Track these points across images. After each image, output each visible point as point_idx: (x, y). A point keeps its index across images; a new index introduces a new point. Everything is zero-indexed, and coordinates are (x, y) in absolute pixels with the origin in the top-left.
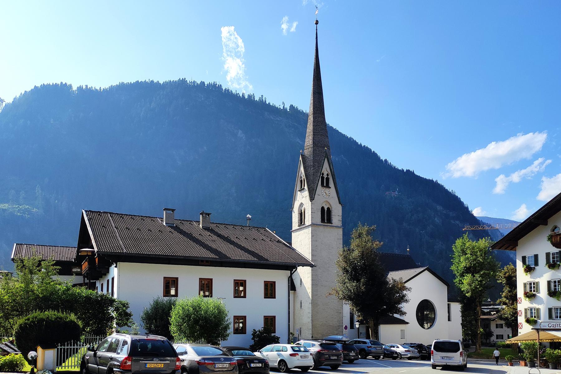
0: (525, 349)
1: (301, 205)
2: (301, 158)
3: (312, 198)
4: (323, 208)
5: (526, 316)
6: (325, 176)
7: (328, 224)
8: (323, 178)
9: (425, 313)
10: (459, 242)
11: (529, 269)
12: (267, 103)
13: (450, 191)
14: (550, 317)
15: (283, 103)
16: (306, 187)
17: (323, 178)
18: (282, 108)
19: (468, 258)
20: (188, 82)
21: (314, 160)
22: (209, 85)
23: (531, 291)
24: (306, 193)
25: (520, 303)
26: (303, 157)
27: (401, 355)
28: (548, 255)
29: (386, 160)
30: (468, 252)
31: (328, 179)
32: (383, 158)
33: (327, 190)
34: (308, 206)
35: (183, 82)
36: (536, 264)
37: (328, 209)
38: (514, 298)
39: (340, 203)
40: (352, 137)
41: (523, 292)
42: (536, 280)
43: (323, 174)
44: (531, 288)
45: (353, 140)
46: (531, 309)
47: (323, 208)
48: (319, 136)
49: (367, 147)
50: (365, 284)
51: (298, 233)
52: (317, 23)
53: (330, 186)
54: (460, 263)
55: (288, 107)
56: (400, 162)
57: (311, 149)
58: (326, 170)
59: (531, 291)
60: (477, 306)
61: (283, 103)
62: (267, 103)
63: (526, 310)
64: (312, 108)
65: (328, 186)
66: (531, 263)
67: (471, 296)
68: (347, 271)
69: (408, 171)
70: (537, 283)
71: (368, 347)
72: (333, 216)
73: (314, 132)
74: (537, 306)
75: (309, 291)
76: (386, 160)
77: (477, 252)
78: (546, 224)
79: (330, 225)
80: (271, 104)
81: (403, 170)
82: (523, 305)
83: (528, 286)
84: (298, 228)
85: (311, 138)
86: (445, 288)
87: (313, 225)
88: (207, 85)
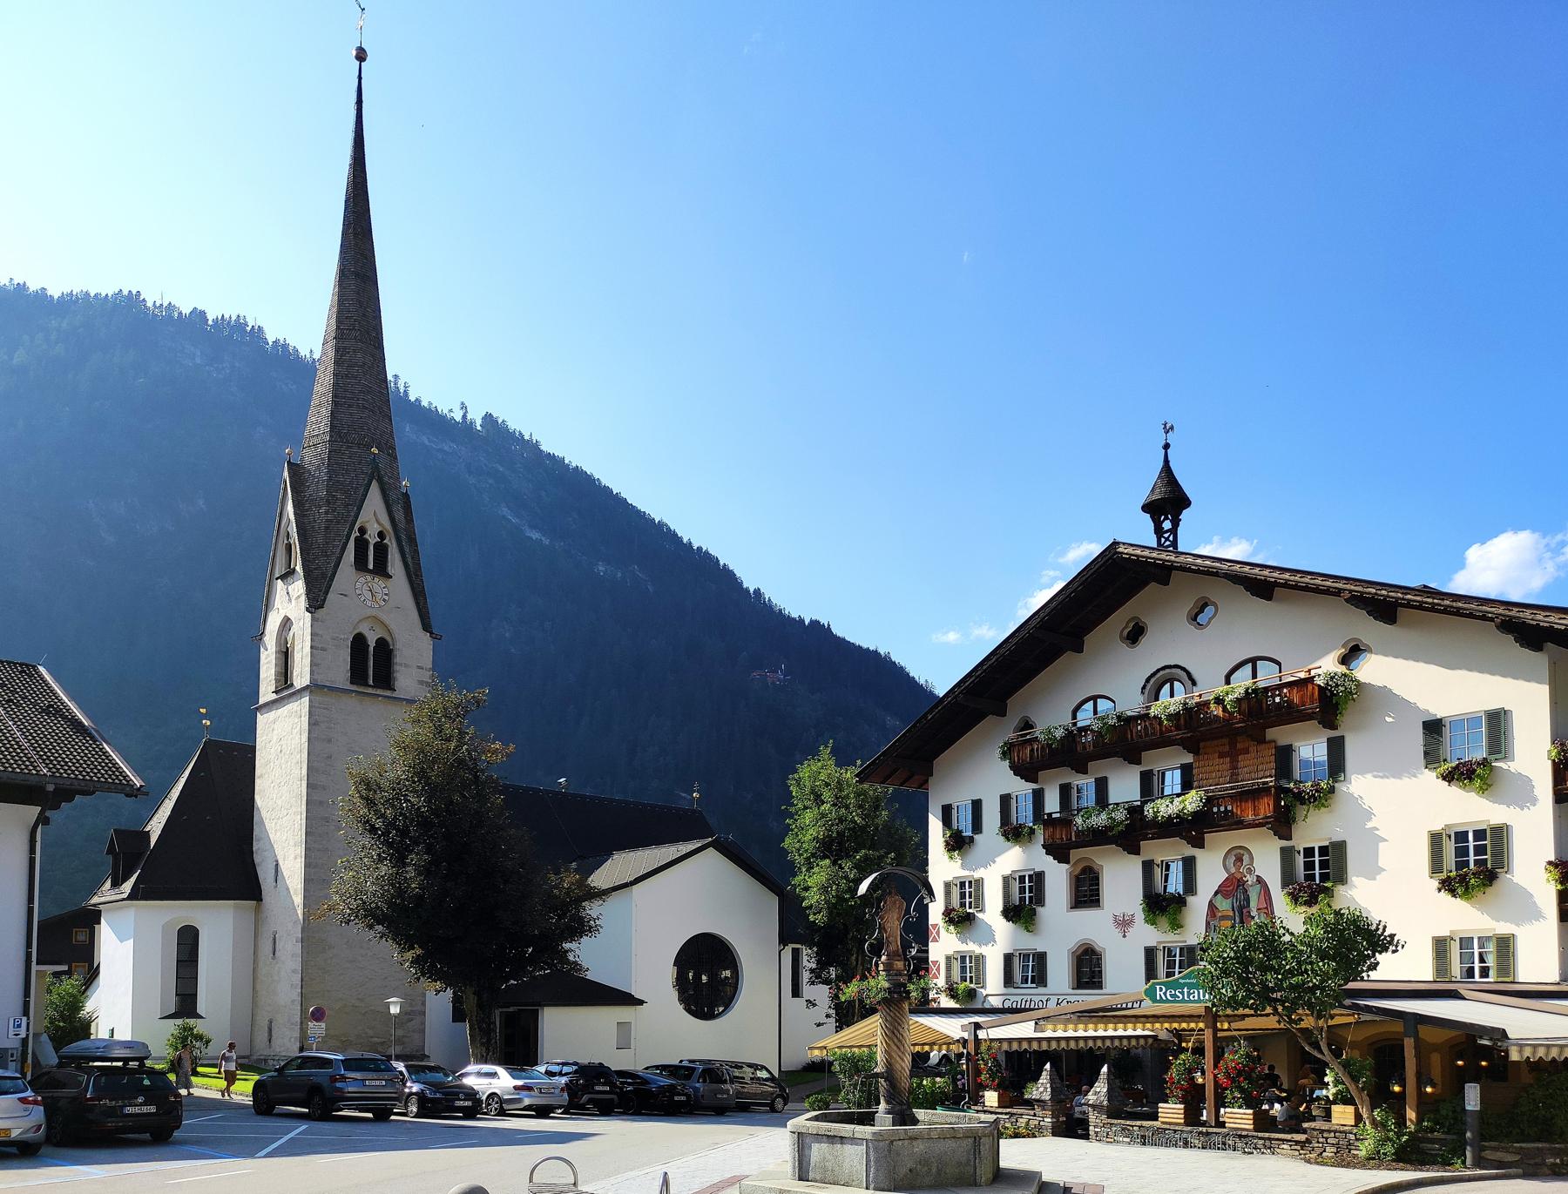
0: (843, 1071)
1: (286, 623)
2: (286, 474)
3: (315, 602)
4: (359, 642)
5: (948, 977)
6: (372, 538)
7: (379, 692)
8: (361, 545)
9: (706, 974)
10: (805, 771)
11: (958, 843)
12: (412, 398)
13: (922, 682)
14: (1008, 980)
15: (463, 406)
16: (299, 568)
17: (361, 545)
18: (458, 418)
19: (823, 815)
20: (150, 304)
21: (332, 484)
22: (221, 323)
23: (963, 905)
24: (298, 587)
25: (935, 940)
26: (296, 470)
27: (501, 1101)
28: (1005, 800)
29: (757, 591)
30: (827, 795)
31: (381, 550)
32: (750, 584)
33: (378, 583)
34: (303, 625)
35: (129, 304)
36: (977, 826)
37: (382, 644)
38: (919, 931)
39: (426, 627)
40: (665, 520)
41: (942, 909)
42: (977, 875)
43: (362, 530)
44: (963, 895)
45: (669, 529)
46: (963, 958)
47: (359, 642)
48: (354, 410)
49: (707, 553)
50: (426, 871)
51: (272, 715)
52: (361, 56)
53: (390, 570)
54: (808, 828)
55: (476, 416)
56: (796, 598)
57: (323, 450)
58: (373, 515)
59: (963, 905)
60: (850, 952)
61: (463, 406)
62: (412, 398)
63: (948, 959)
64: (333, 321)
65: (381, 570)
66: (964, 823)
67: (828, 927)
68: (373, 830)
69: (815, 624)
70: (977, 881)
71: (333, 1079)
72: (396, 668)
73: (335, 396)
74: (972, 947)
75: (298, 900)
76: (757, 591)
77: (847, 797)
78: (1002, 713)
79: (388, 693)
80: (425, 403)
81: (802, 621)
82: (944, 945)
83: (956, 892)
84: (274, 696)
85: (325, 412)
86: (774, 902)
87: (313, 688)
88: (216, 321)
